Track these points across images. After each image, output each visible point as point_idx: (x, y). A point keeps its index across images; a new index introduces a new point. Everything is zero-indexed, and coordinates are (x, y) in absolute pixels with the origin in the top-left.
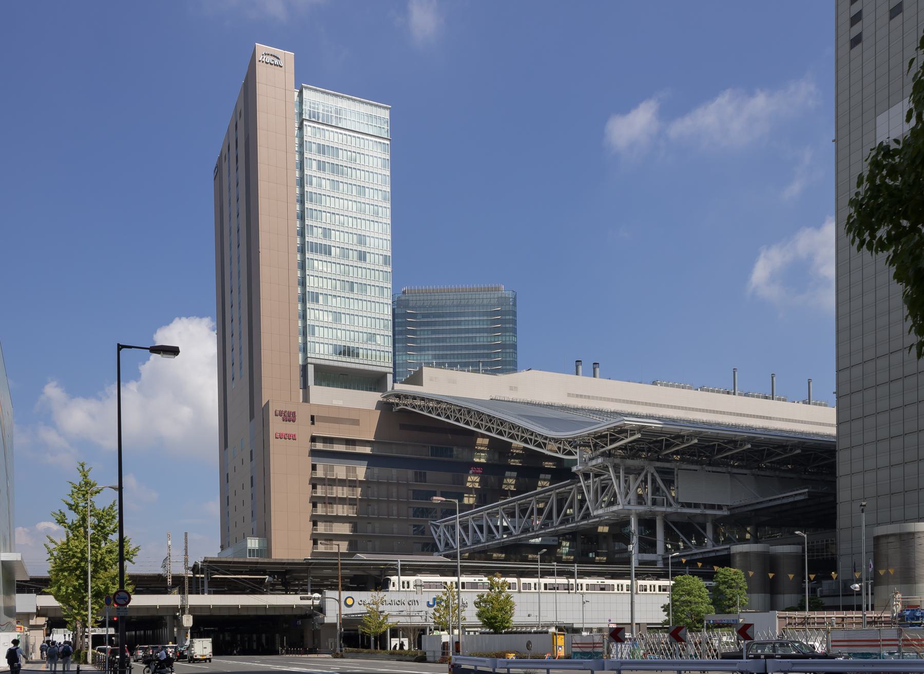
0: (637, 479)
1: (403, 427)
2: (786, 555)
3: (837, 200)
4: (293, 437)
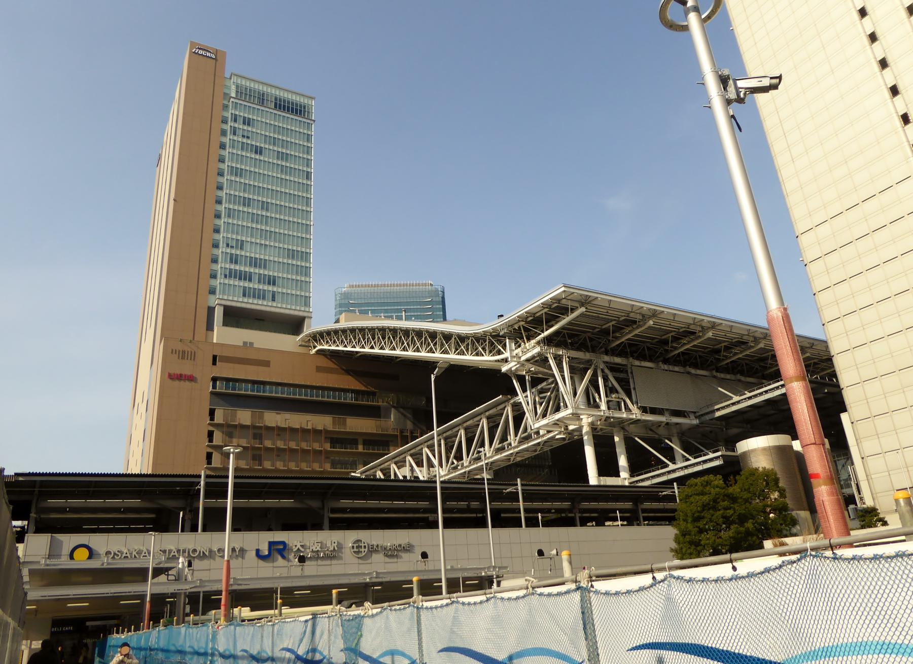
4: (191, 379)
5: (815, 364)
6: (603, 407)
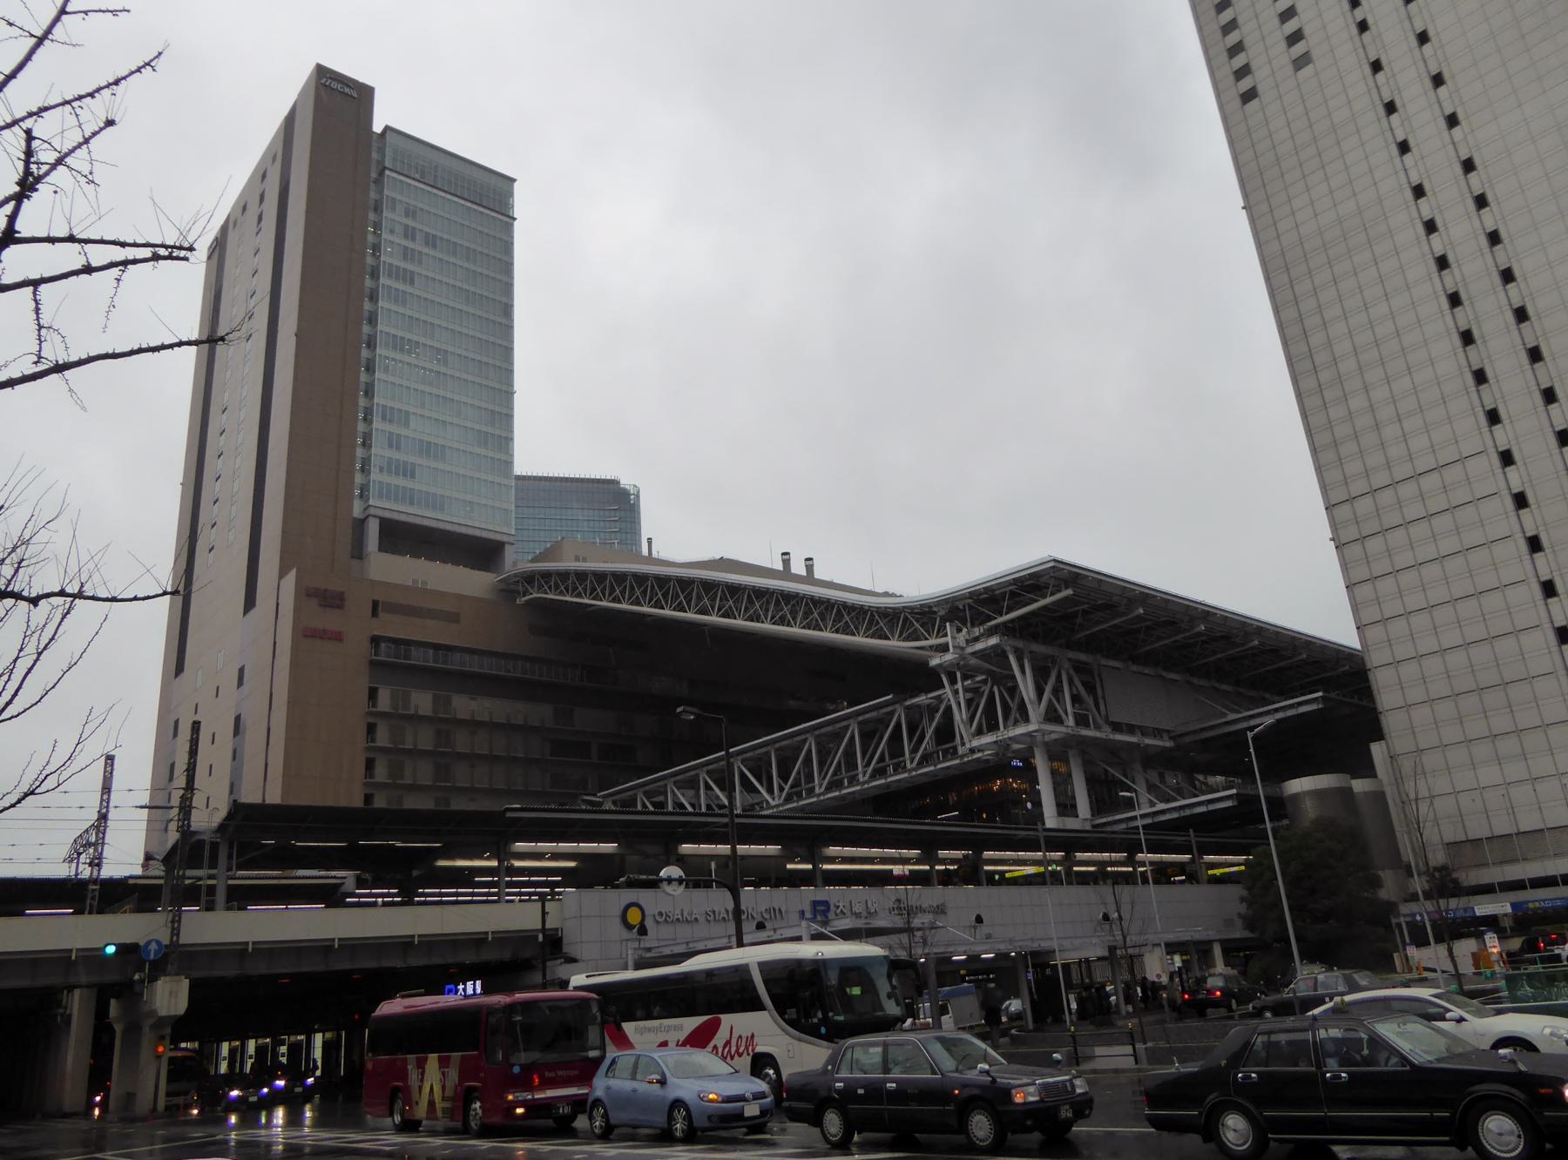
3: (1268, 279)
4: (338, 637)
5: (1147, 628)
6: (1071, 721)
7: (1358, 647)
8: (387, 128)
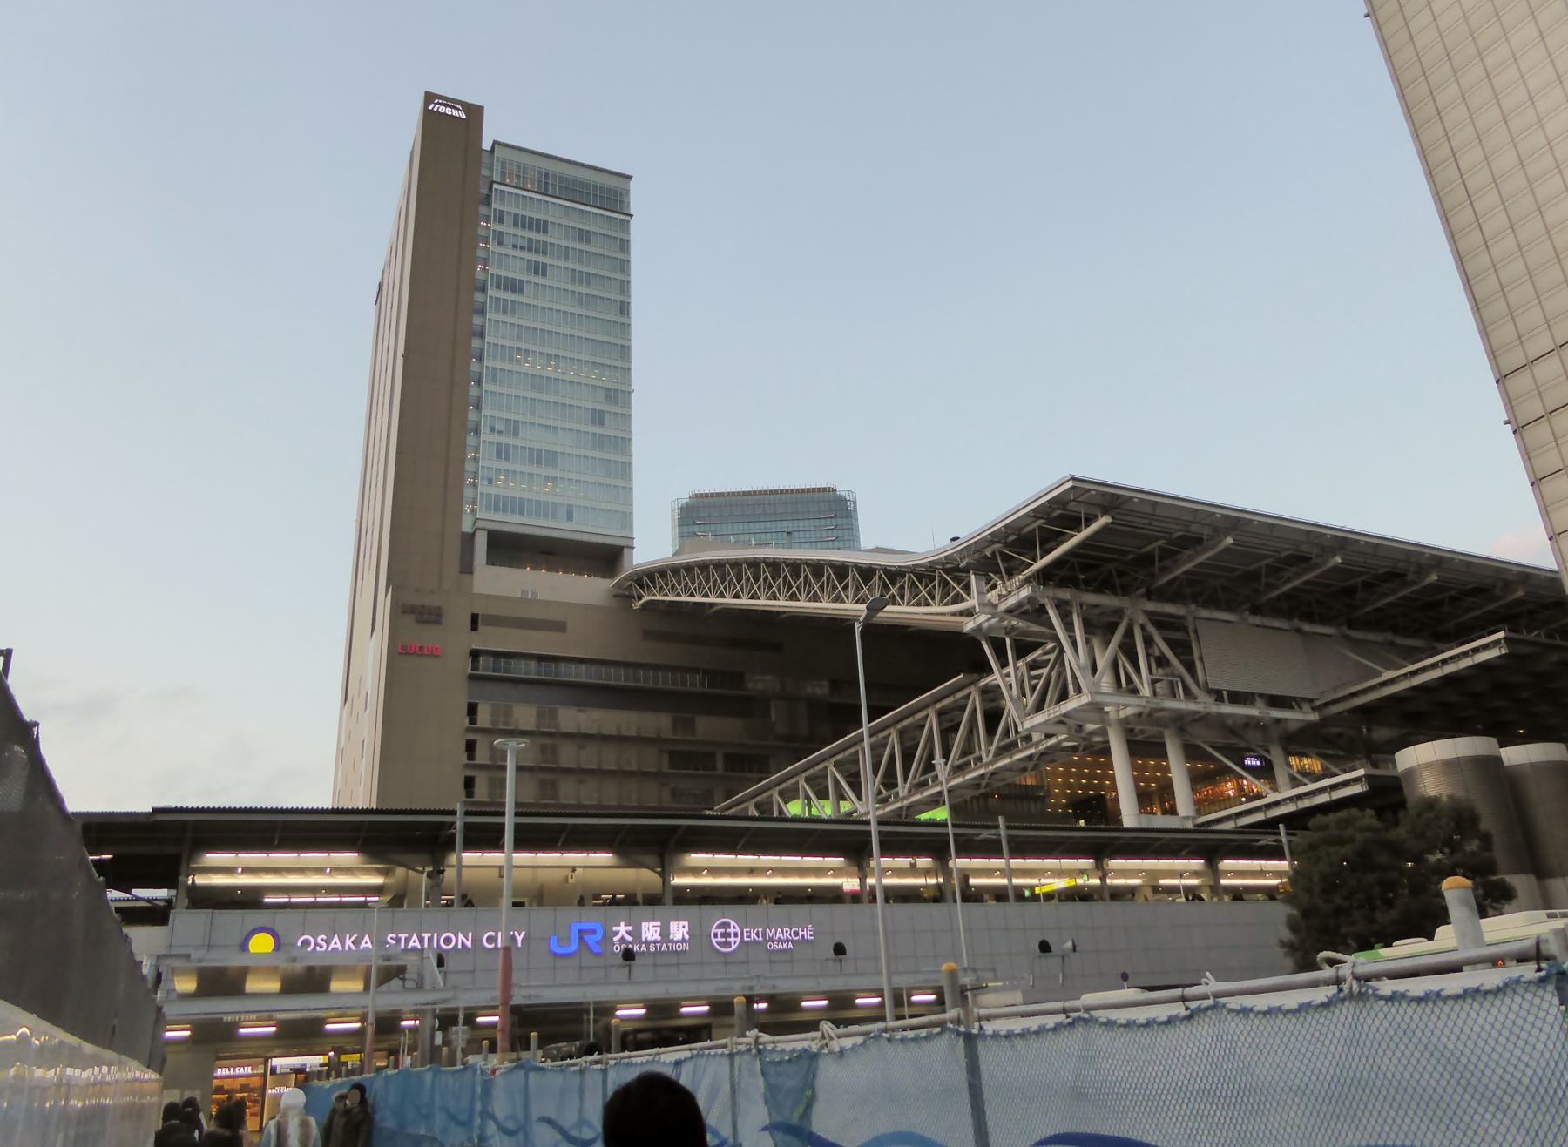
0: (1107, 643)
1: (648, 635)
2: (1535, 767)
4: (434, 654)
6: (1146, 691)
7: (1554, 567)
8: (495, 143)
